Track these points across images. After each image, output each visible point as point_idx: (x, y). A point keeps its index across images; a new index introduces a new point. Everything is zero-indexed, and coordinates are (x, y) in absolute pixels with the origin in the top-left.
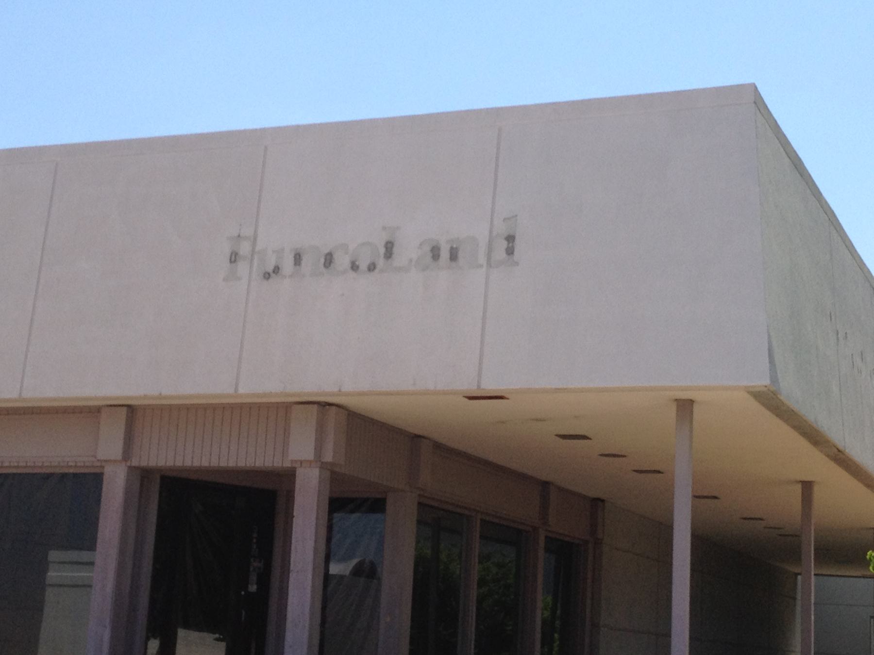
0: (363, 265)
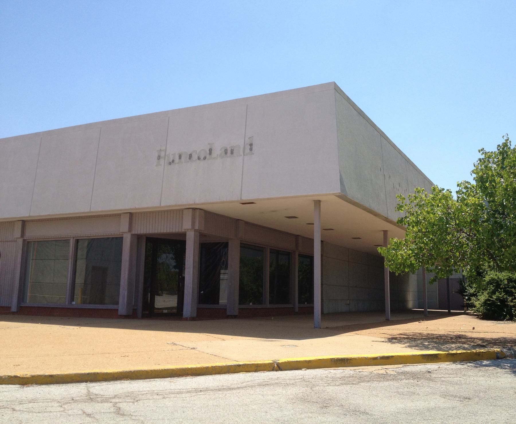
0: (202, 158)
